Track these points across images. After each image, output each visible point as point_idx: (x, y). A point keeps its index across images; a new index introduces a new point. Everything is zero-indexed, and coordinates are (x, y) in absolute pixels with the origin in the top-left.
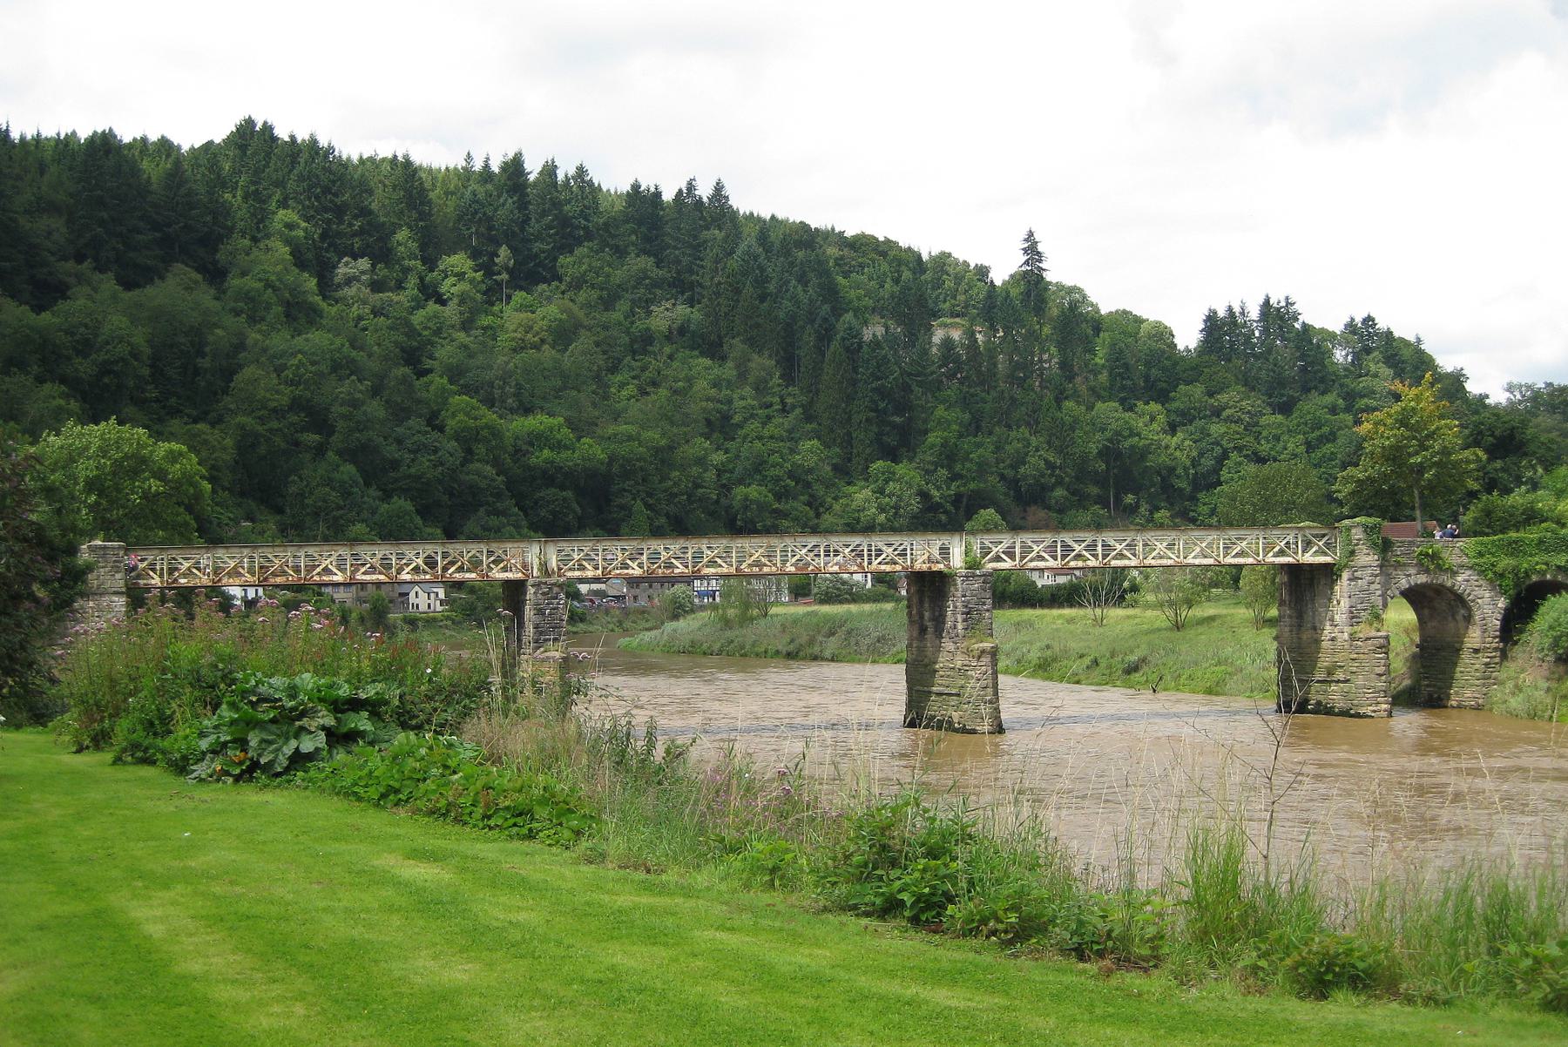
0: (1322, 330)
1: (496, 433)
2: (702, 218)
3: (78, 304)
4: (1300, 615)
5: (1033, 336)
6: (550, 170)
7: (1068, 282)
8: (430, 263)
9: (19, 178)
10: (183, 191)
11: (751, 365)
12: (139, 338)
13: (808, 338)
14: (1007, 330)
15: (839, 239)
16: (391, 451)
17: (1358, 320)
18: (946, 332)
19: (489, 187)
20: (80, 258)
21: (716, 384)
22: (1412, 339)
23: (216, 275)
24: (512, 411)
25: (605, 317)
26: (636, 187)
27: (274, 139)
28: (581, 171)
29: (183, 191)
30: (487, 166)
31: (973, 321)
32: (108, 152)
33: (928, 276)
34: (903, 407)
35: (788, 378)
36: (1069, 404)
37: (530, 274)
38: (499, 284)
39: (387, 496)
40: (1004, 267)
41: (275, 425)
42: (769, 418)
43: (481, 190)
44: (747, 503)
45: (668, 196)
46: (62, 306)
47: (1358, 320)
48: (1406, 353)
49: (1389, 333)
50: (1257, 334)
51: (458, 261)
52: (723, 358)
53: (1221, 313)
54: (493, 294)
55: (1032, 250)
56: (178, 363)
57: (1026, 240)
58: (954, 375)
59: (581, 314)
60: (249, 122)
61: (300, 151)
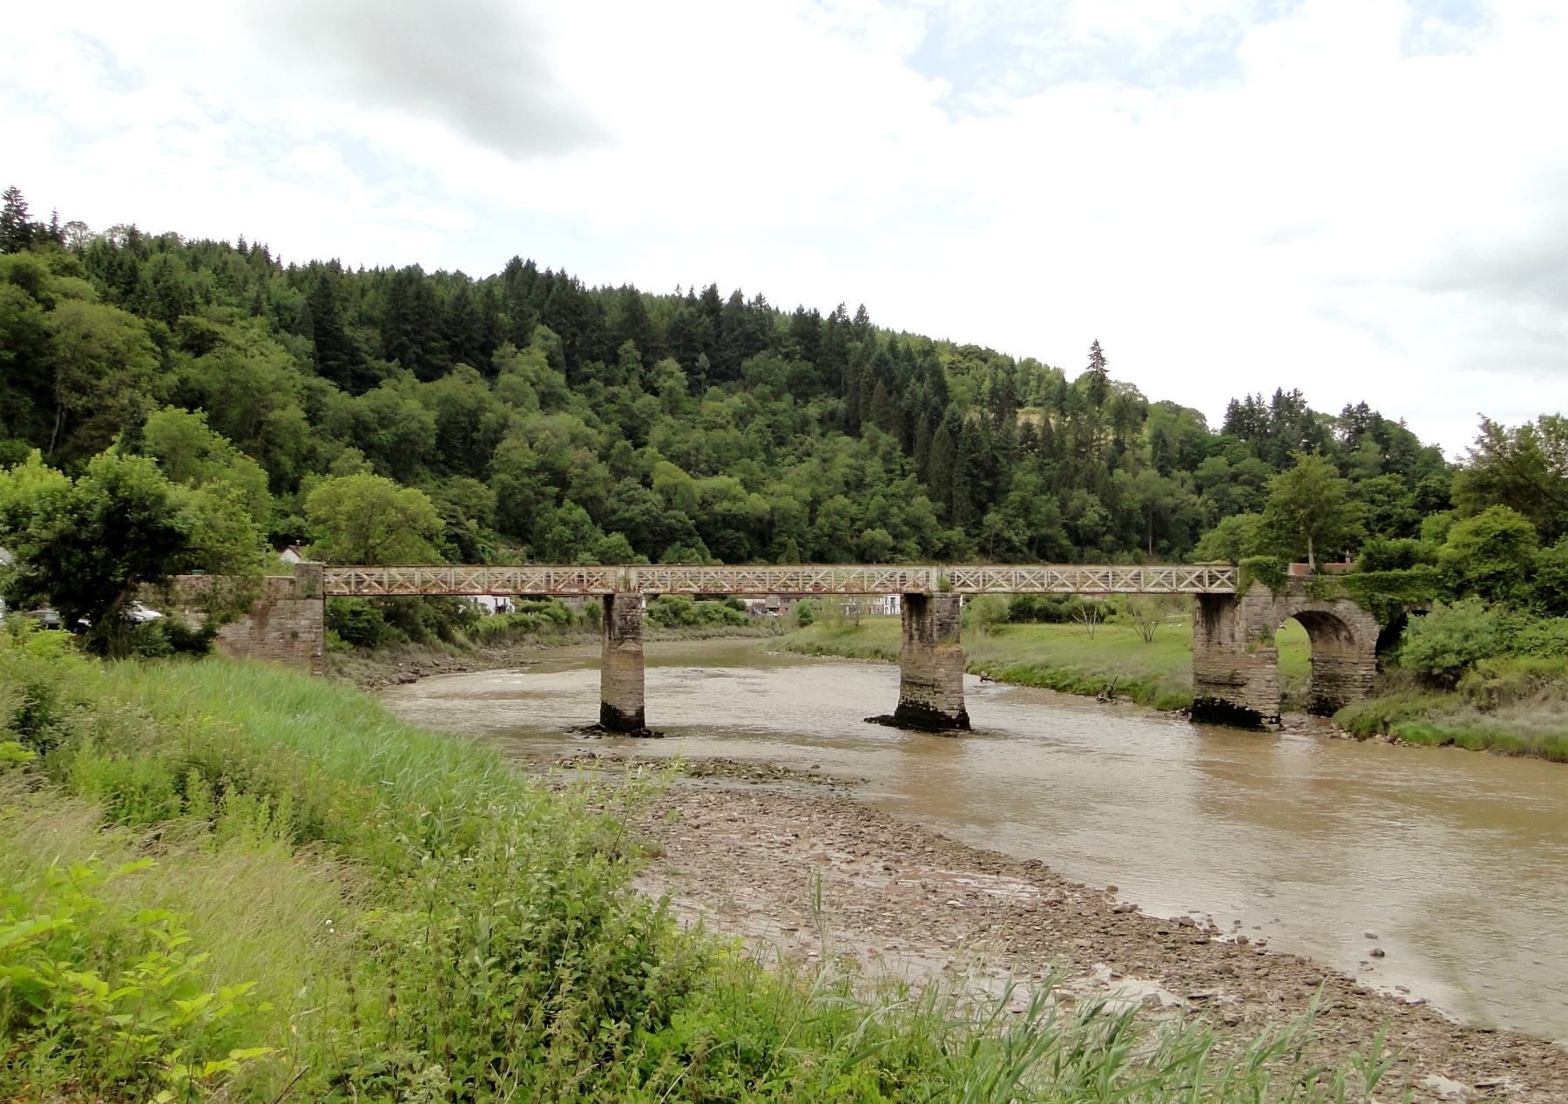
0: (1324, 415)
1: (689, 489)
2: (849, 333)
3: (382, 395)
4: (1209, 633)
5: (1094, 421)
6: (737, 297)
7: (1124, 380)
8: (648, 366)
9: (346, 300)
10: (468, 309)
11: (880, 441)
12: (430, 418)
13: (922, 424)
14: (1074, 415)
15: (953, 349)
16: (612, 502)
17: (1354, 406)
18: (1030, 416)
19: (692, 309)
20: (389, 359)
21: (855, 456)
22: (1398, 421)
23: (491, 372)
24: (703, 473)
25: (774, 405)
26: (800, 310)
27: (534, 272)
28: (760, 299)
29: (468, 309)
30: (692, 294)
31: (1048, 411)
32: (411, 281)
33: (1018, 376)
34: (992, 474)
35: (908, 451)
36: (1119, 472)
37: (724, 374)
38: (699, 381)
39: (607, 533)
40: (1074, 369)
41: (526, 480)
42: (891, 480)
43: (686, 312)
44: (873, 542)
45: (825, 315)
46: (372, 393)
47: (1354, 406)
48: (1393, 432)
49: (1377, 417)
50: (1271, 417)
51: (670, 364)
52: (860, 436)
53: (1242, 403)
54: (695, 389)
55: (1097, 356)
56: (460, 435)
57: (1093, 348)
58: (1032, 449)
59: (757, 404)
60: (517, 261)
61: (553, 283)
